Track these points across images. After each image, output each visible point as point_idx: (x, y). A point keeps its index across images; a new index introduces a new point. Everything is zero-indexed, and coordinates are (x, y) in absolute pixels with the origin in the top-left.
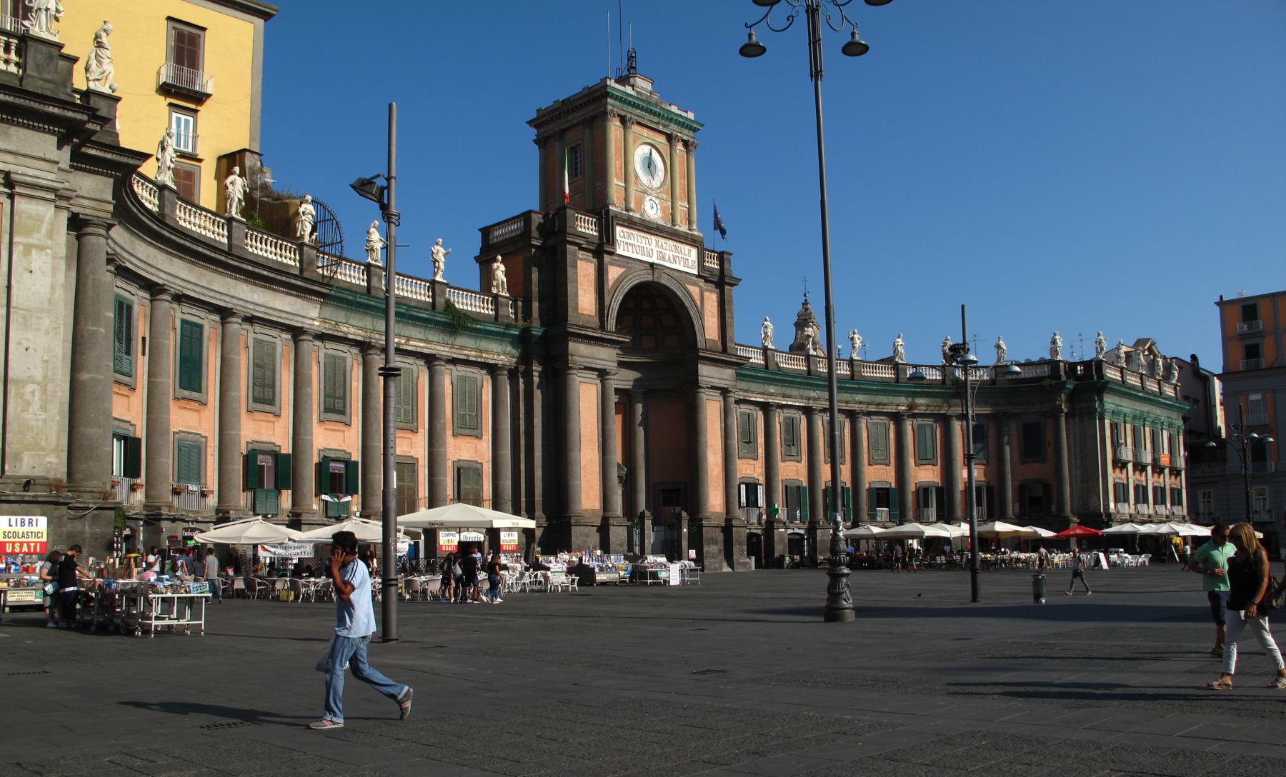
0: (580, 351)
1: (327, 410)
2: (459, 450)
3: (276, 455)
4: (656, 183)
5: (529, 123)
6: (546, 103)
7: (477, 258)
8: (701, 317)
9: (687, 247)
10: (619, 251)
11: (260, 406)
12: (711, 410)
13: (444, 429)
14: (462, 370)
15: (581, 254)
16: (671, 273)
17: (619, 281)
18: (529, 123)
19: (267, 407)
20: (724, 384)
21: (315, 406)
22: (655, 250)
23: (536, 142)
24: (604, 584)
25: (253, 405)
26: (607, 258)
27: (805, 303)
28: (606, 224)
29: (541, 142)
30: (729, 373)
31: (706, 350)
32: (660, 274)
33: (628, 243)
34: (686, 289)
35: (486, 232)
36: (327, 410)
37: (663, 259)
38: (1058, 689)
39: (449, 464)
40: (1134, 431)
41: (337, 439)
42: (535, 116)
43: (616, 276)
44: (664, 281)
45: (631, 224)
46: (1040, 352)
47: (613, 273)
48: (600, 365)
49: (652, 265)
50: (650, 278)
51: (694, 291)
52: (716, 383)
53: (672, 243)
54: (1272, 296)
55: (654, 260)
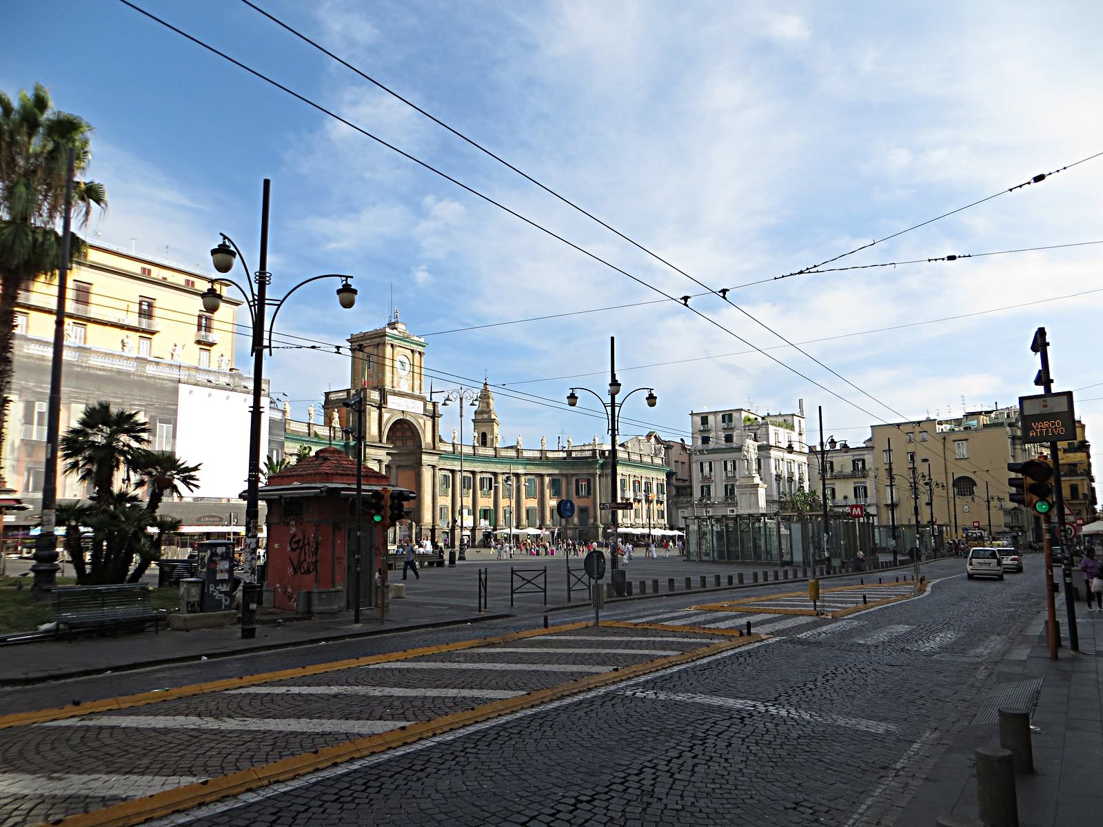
12: (427, 474)
30: (436, 458)
45: (395, 394)
47: (386, 416)
51: (421, 421)
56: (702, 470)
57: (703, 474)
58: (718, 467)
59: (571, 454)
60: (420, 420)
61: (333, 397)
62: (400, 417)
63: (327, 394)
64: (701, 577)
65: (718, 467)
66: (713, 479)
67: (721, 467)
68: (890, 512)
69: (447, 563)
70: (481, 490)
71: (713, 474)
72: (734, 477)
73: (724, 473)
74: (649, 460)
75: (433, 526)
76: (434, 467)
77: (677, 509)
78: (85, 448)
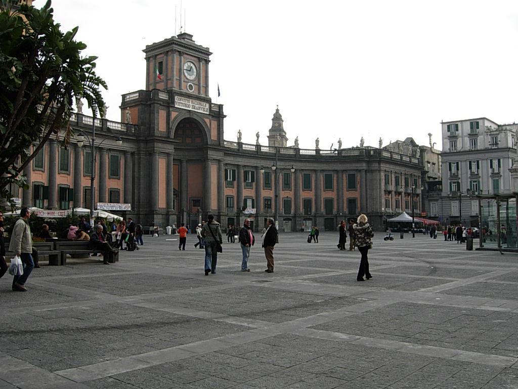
0: (159, 146)
1: (326, 188)
2: (112, 184)
3: (44, 187)
4: (192, 77)
5: (143, 51)
6: (150, 43)
7: (120, 107)
8: (210, 131)
9: (205, 103)
10: (176, 106)
11: (37, 169)
12: (213, 170)
13: (105, 176)
14: (113, 153)
15: (161, 107)
16: (197, 114)
17: (176, 118)
18: (143, 51)
19: (40, 169)
20: (219, 158)
21: (301, 186)
22: (191, 105)
23: (145, 58)
24: (176, 108)
25: (348, 189)
26: (171, 109)
27: (277, 110)
28: (171, 94)
29: (147, 59)
30: (221, 154)
31: (211, 145)
32: (193, 115)
33: (181, 103)
34: (204, 120)
35: (124, 96)
36: (326, 188)
37: (195, 108)
38: (296, 253)
39: (107, 189)
40: (396, 177)
41: (63, 180)
42: (145, 48)
43: (175, 116)
44: (195, 117)
45: (181, 95)
46: (357, 144)
47: (174, 115)
48: (167, 151)
49: (190, 111)
50: (189, 116)
51: (207, 121)
52: (215, 157)
53: (198, 102)
54: (461, 121)
55: (190, 109)
56: (450, 170)
57: (471, 171)
58: (464, 166)
59: (341, 154)
60: (206, 120)
61: (128, 98)
62: (187, 116)
63: (124, 96)
64: (310, 242)
65: (464, 166)
66: (460, 176)
67: (466, 165)
68: (12, 193)
69: (170, 233)
70: (245, 181)
71: (480, 171)
72: (478, 174)
73: (449, 172)
74: (408, 159)
75: (219, 213)
76: (219, 161)
77: (429, 201)
78: (35, 82)
